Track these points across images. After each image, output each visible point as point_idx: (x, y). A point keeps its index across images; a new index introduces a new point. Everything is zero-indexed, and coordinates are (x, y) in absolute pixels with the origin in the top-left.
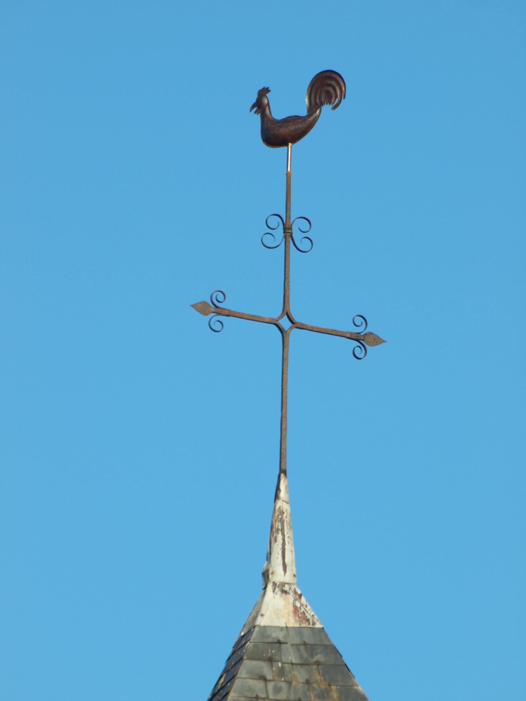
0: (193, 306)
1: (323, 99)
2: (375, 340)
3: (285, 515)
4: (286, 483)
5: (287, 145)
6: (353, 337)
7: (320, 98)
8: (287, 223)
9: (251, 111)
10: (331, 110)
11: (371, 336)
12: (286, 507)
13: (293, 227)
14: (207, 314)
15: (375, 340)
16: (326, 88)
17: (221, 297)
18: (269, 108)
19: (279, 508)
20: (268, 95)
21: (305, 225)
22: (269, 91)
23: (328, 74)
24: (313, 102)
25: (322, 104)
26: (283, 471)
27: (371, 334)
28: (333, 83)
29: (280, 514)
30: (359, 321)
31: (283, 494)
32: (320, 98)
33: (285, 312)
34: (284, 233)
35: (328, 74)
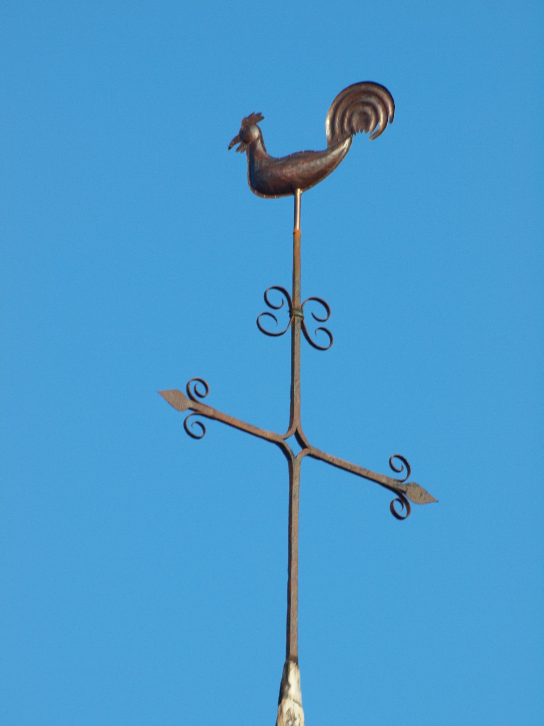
0: (161, 393)
1: (354, 124)
2: (421, 495)
3: (297, 722)
4: (298, 674)
5: (294, 193)
6: (391, 484)
7: (350, 122)
8: (296, 303)
9: (230, 148)
10: (370, 140)
11: (417, 488)
12: (298, 711)
13: (304, 308)
14: (183, 410)
15: (421, 495)
16: (361, 108)
17: (201, 389)
18: (262, 142)
19: (289, 710)
20: (259, 124)
21: (321, 312)
22: (262, 118)
23: (363, 87)
24: (337, 130)
25: (353, 132)
26: (290, 658)
27: (415, 485)
28: (373, 100)
29: (291, 719)
30: (398, 464)
31: (294, 690)
32: (350, 122)
33: (294, 429)
34: (291, 316)
35: (363, 87)
